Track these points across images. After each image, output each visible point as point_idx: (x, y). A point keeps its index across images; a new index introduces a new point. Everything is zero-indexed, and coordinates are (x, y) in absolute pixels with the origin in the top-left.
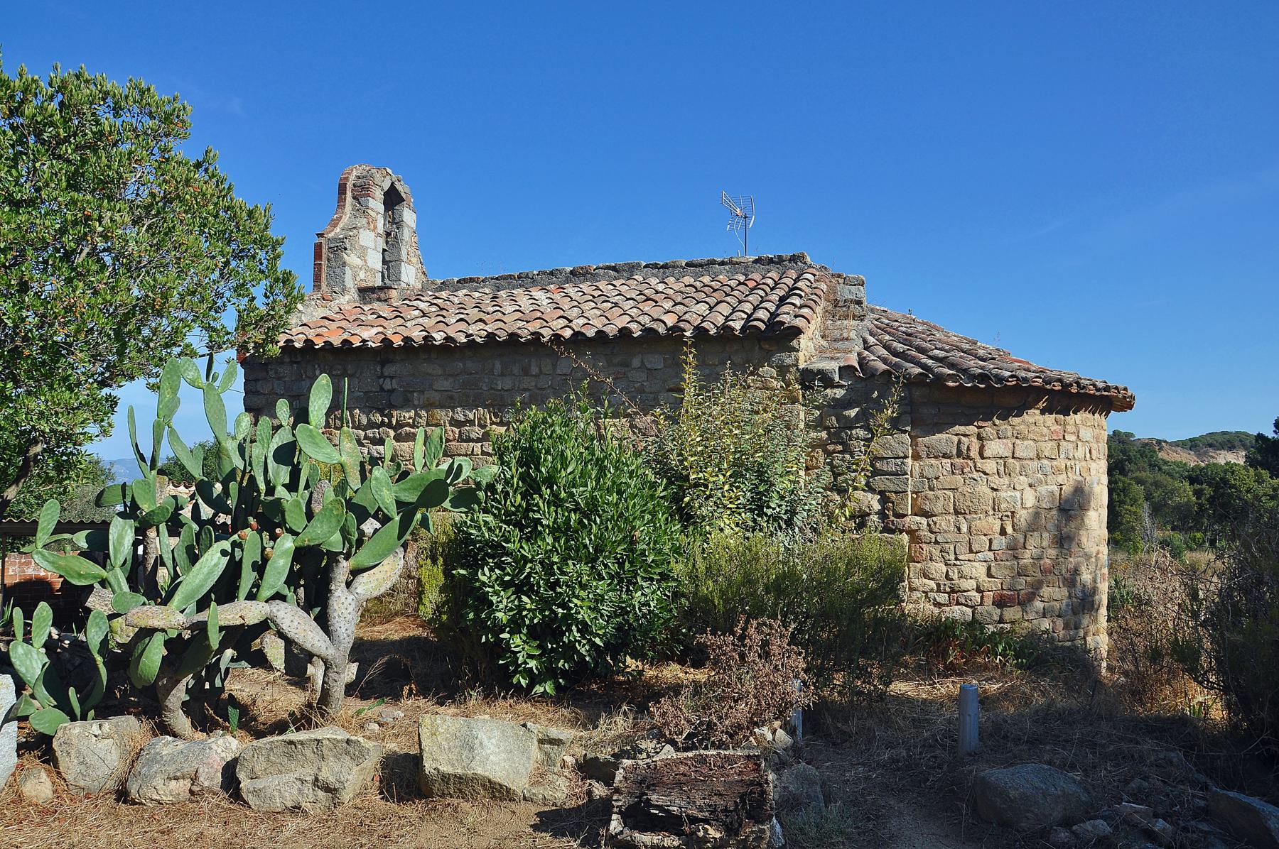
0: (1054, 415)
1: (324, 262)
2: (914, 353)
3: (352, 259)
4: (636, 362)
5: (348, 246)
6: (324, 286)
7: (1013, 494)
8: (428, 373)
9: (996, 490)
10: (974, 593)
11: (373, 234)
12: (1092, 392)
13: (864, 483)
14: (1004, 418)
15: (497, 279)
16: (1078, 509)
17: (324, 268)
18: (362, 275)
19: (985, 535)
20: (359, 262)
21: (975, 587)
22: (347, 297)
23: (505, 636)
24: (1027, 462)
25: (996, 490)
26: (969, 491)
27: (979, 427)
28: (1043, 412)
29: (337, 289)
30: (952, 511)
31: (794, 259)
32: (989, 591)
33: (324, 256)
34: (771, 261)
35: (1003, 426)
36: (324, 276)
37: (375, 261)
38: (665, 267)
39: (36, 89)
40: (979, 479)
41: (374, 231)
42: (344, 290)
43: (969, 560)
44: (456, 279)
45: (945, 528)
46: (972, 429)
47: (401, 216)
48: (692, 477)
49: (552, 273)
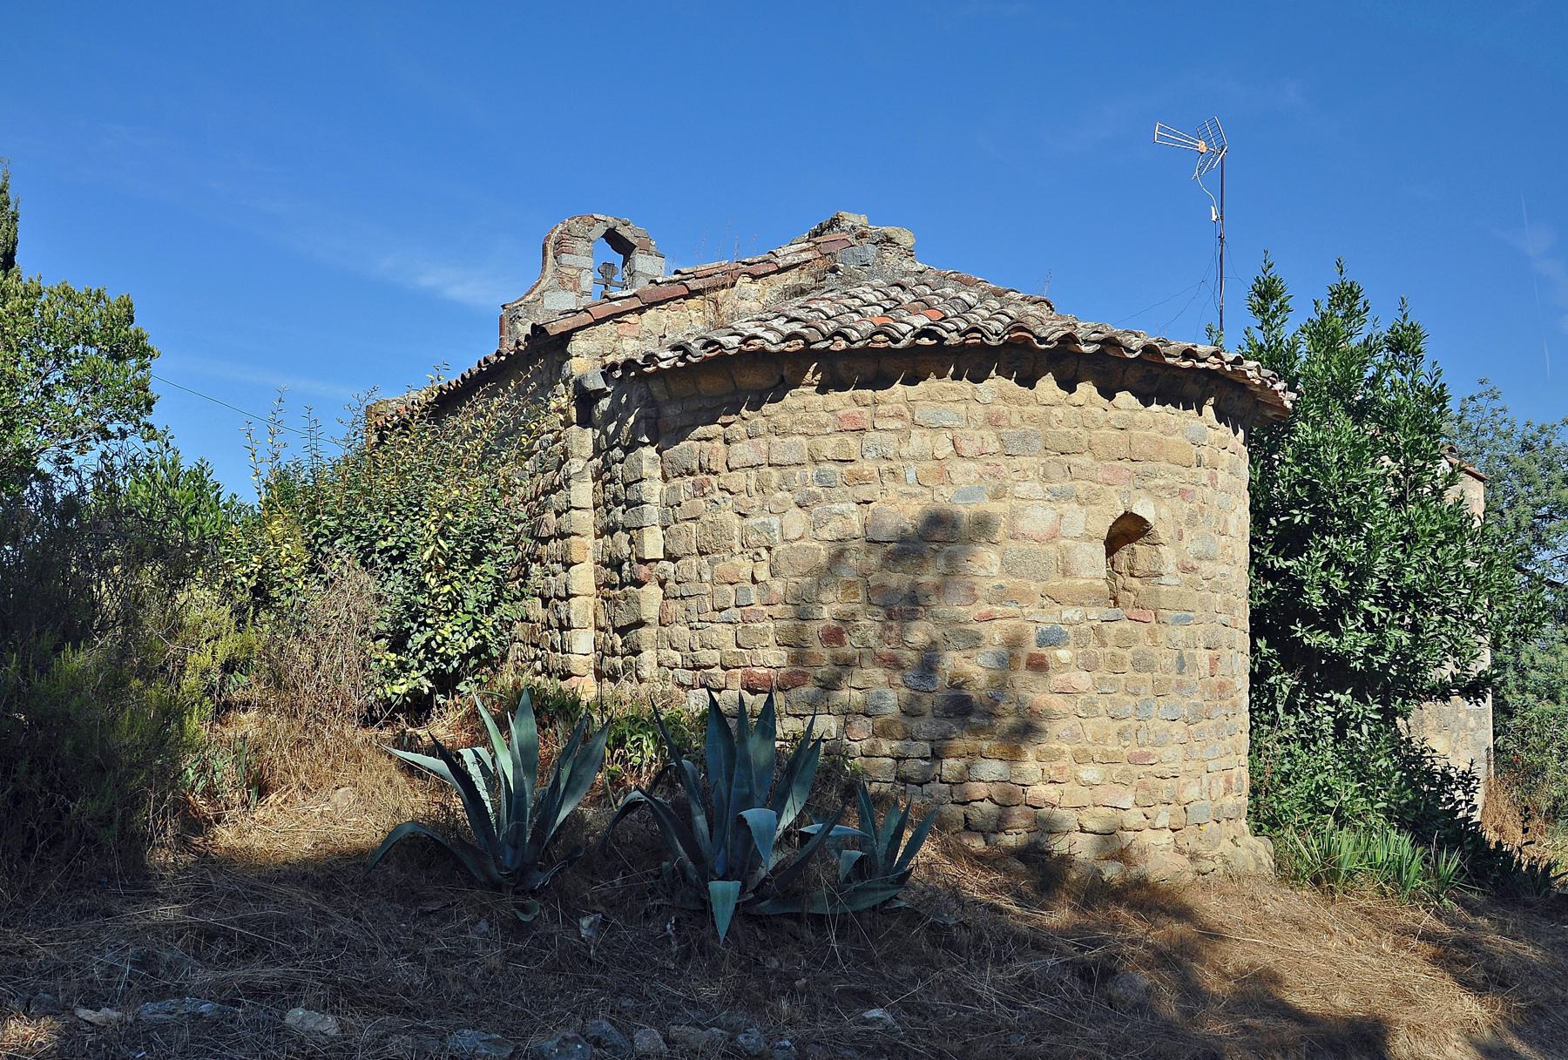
0: (850, 392)
2: (892, 323)
7: (766, 520)
8: (974, 994)
9: (744, 516)
10: (717, 670)
12: (882, 345)
14: (755, 406)
16: (1125, 571)
19: (731, 584)
21: (718, 661)
23: (58, 496)
24: (793, 469)
25: (744, 516)
26: (710, 519)
27: (725, 425)
28: (822, 389)
30: (695, 551)
32: (735, 667)
35: (756, 419)
40: (720, 501)
42: (1285, 560)
43: (711, 622)
45: (688, 576)
46: (715, 429)
48: (787, 726)
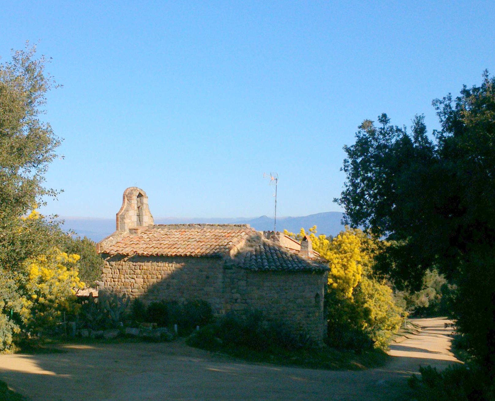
1: (119, 222)
3: (127, 221)
4: (189, 262)
5: (126, 217)
6: (119, 229)
11: (133, 211)
13: (373, 150)
15: (169, 225)
17: (119, 224)
18: (130, 224)
20: (129, 221)
22: (126, 232)
29: (123, 230)
31: (244, 226)
33: (119, 220)
34: (238, 226)
36: (119, 226)
37: (135, 218)
38: (212, 225)
39: (45, 298)
41: (134, 210)
44: (158, 224)
47: (143, 201)
49: (183, 225)
